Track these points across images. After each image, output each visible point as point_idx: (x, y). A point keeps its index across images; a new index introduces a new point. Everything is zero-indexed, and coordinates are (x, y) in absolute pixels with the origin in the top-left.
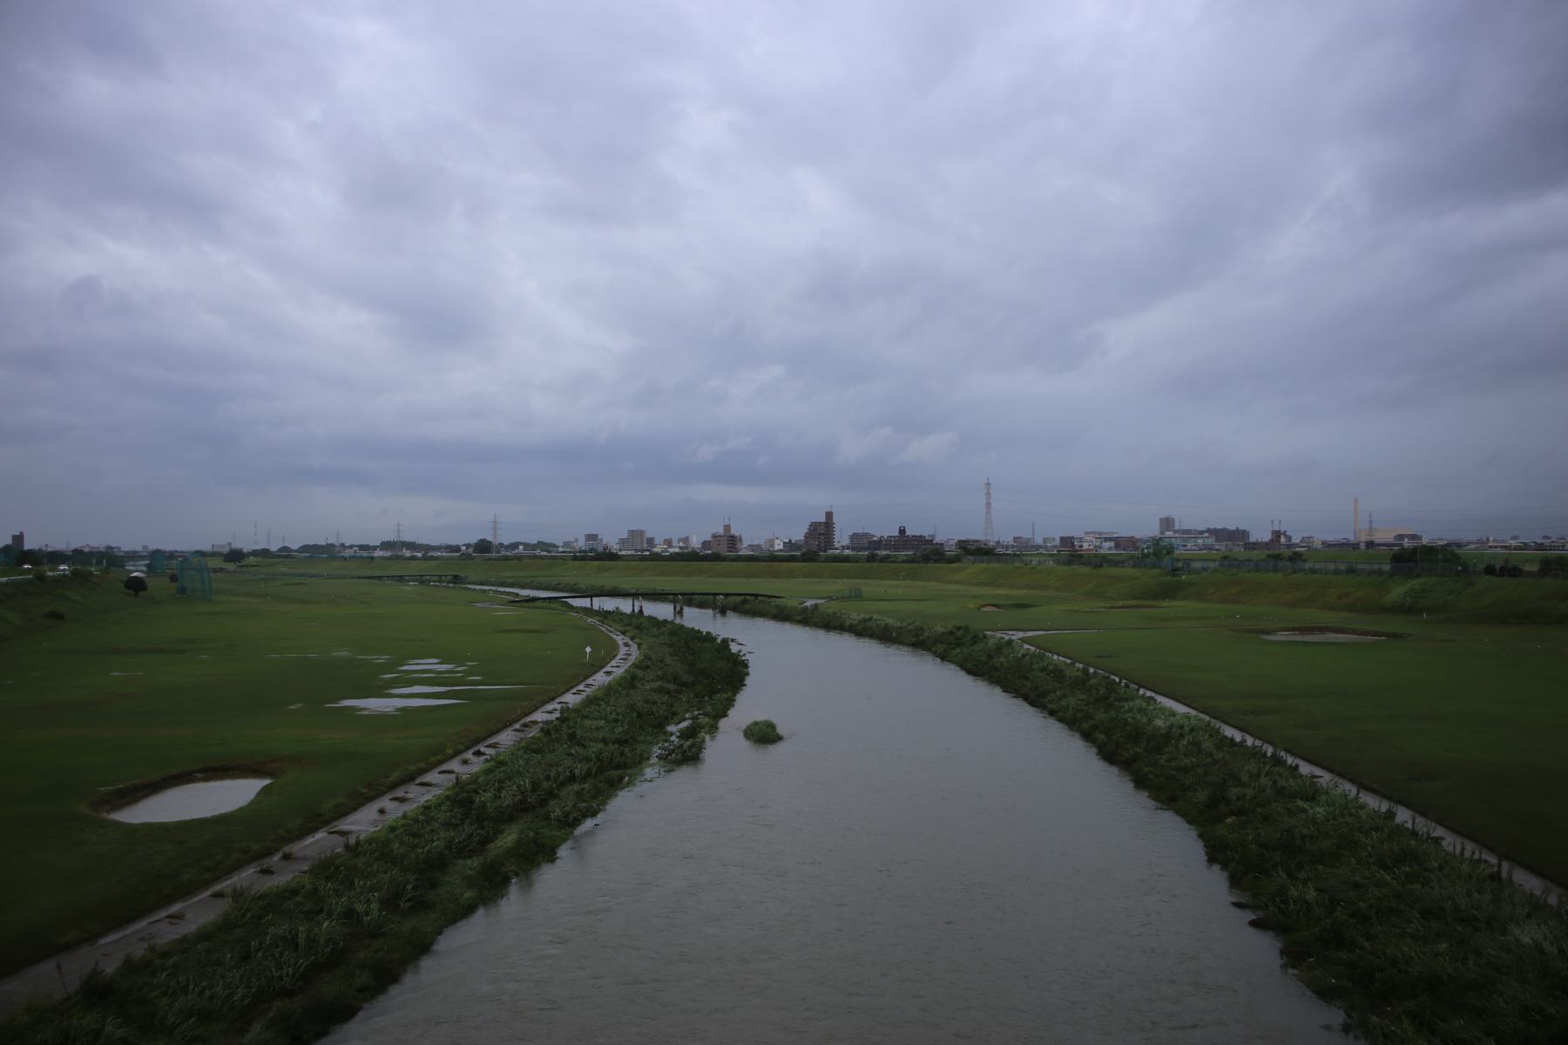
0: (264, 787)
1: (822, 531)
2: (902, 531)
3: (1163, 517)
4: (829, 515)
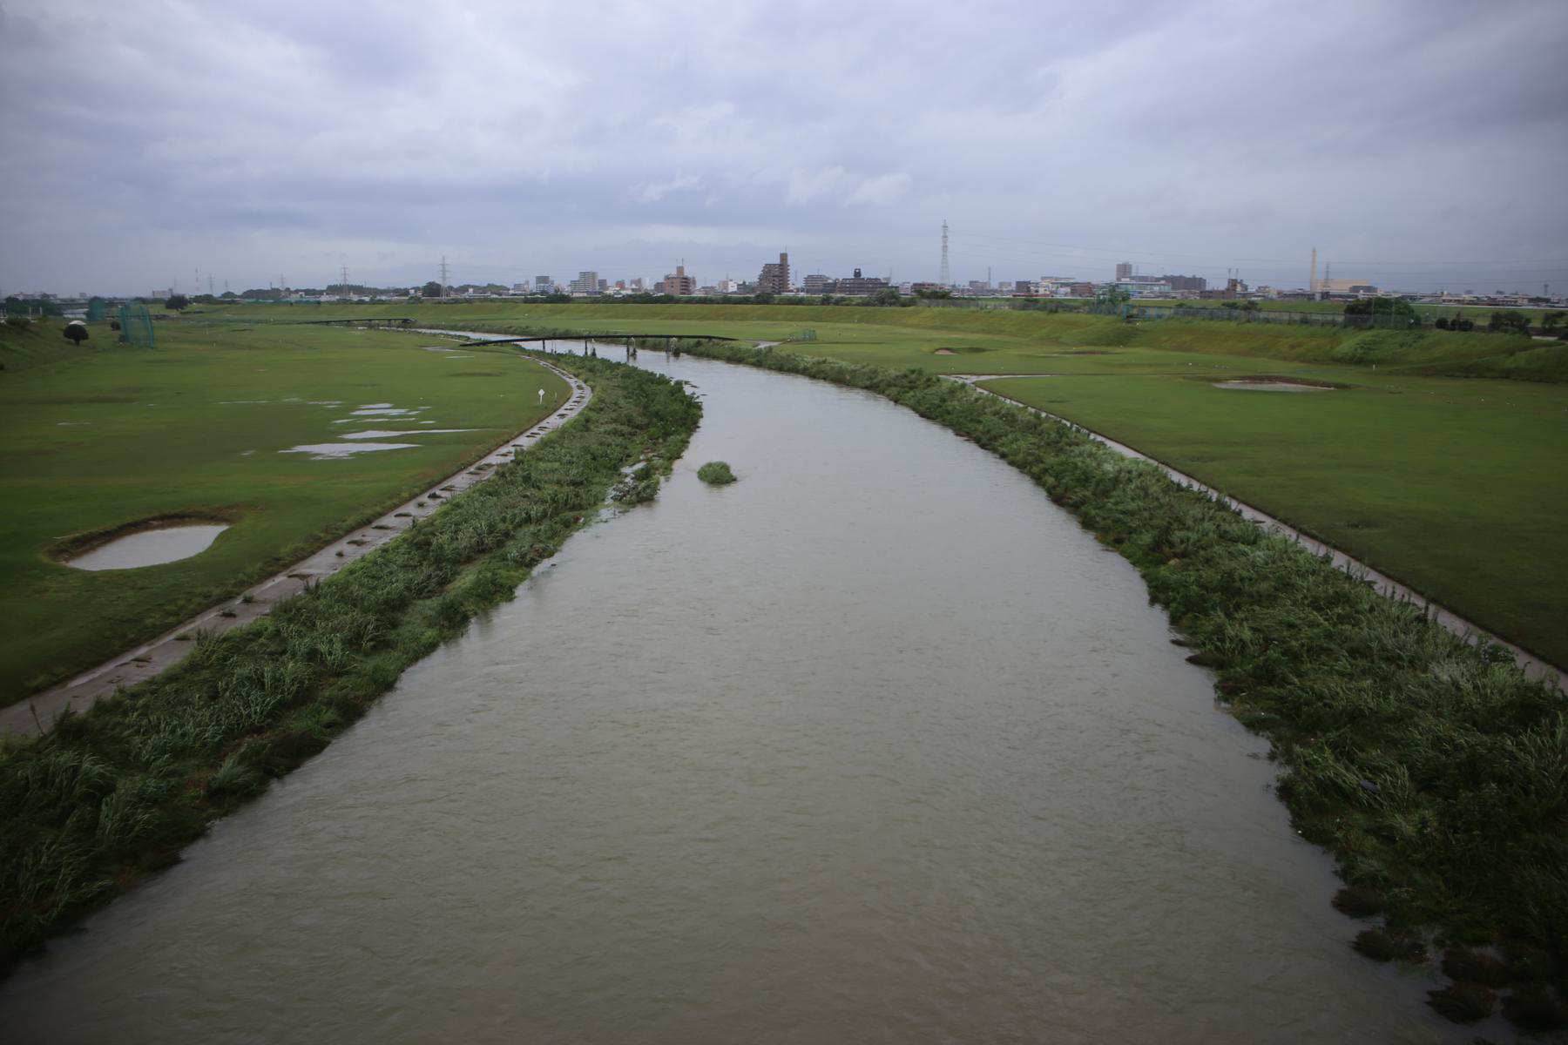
1: (777, 273)
2: (857, 274)
4: (784, 257)
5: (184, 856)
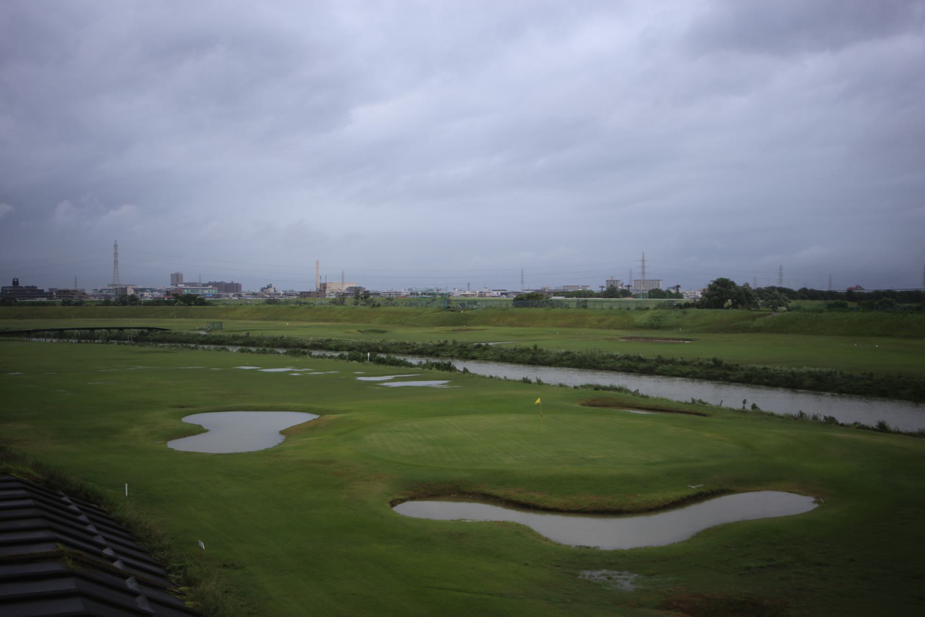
0: (314, 419)
2: (16, 283)
3: (174, 273)
5: (280, 439)
